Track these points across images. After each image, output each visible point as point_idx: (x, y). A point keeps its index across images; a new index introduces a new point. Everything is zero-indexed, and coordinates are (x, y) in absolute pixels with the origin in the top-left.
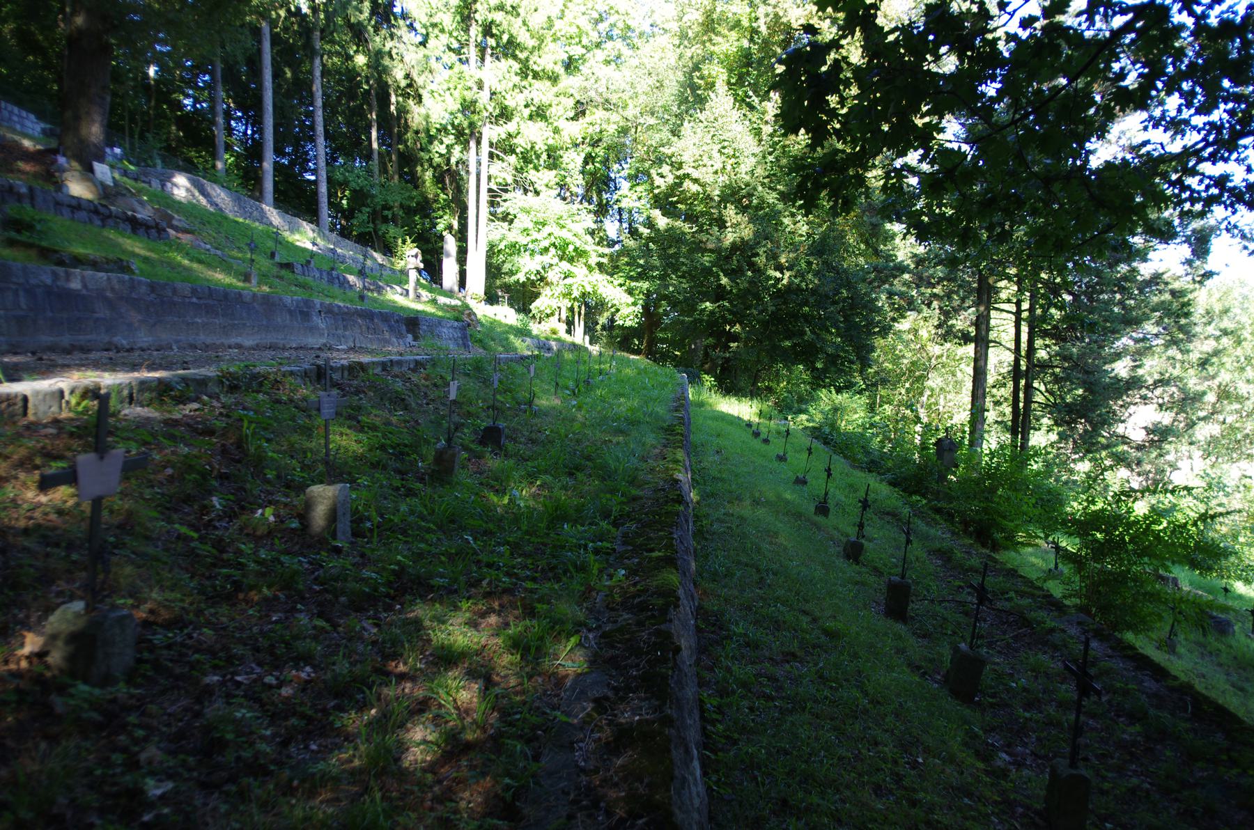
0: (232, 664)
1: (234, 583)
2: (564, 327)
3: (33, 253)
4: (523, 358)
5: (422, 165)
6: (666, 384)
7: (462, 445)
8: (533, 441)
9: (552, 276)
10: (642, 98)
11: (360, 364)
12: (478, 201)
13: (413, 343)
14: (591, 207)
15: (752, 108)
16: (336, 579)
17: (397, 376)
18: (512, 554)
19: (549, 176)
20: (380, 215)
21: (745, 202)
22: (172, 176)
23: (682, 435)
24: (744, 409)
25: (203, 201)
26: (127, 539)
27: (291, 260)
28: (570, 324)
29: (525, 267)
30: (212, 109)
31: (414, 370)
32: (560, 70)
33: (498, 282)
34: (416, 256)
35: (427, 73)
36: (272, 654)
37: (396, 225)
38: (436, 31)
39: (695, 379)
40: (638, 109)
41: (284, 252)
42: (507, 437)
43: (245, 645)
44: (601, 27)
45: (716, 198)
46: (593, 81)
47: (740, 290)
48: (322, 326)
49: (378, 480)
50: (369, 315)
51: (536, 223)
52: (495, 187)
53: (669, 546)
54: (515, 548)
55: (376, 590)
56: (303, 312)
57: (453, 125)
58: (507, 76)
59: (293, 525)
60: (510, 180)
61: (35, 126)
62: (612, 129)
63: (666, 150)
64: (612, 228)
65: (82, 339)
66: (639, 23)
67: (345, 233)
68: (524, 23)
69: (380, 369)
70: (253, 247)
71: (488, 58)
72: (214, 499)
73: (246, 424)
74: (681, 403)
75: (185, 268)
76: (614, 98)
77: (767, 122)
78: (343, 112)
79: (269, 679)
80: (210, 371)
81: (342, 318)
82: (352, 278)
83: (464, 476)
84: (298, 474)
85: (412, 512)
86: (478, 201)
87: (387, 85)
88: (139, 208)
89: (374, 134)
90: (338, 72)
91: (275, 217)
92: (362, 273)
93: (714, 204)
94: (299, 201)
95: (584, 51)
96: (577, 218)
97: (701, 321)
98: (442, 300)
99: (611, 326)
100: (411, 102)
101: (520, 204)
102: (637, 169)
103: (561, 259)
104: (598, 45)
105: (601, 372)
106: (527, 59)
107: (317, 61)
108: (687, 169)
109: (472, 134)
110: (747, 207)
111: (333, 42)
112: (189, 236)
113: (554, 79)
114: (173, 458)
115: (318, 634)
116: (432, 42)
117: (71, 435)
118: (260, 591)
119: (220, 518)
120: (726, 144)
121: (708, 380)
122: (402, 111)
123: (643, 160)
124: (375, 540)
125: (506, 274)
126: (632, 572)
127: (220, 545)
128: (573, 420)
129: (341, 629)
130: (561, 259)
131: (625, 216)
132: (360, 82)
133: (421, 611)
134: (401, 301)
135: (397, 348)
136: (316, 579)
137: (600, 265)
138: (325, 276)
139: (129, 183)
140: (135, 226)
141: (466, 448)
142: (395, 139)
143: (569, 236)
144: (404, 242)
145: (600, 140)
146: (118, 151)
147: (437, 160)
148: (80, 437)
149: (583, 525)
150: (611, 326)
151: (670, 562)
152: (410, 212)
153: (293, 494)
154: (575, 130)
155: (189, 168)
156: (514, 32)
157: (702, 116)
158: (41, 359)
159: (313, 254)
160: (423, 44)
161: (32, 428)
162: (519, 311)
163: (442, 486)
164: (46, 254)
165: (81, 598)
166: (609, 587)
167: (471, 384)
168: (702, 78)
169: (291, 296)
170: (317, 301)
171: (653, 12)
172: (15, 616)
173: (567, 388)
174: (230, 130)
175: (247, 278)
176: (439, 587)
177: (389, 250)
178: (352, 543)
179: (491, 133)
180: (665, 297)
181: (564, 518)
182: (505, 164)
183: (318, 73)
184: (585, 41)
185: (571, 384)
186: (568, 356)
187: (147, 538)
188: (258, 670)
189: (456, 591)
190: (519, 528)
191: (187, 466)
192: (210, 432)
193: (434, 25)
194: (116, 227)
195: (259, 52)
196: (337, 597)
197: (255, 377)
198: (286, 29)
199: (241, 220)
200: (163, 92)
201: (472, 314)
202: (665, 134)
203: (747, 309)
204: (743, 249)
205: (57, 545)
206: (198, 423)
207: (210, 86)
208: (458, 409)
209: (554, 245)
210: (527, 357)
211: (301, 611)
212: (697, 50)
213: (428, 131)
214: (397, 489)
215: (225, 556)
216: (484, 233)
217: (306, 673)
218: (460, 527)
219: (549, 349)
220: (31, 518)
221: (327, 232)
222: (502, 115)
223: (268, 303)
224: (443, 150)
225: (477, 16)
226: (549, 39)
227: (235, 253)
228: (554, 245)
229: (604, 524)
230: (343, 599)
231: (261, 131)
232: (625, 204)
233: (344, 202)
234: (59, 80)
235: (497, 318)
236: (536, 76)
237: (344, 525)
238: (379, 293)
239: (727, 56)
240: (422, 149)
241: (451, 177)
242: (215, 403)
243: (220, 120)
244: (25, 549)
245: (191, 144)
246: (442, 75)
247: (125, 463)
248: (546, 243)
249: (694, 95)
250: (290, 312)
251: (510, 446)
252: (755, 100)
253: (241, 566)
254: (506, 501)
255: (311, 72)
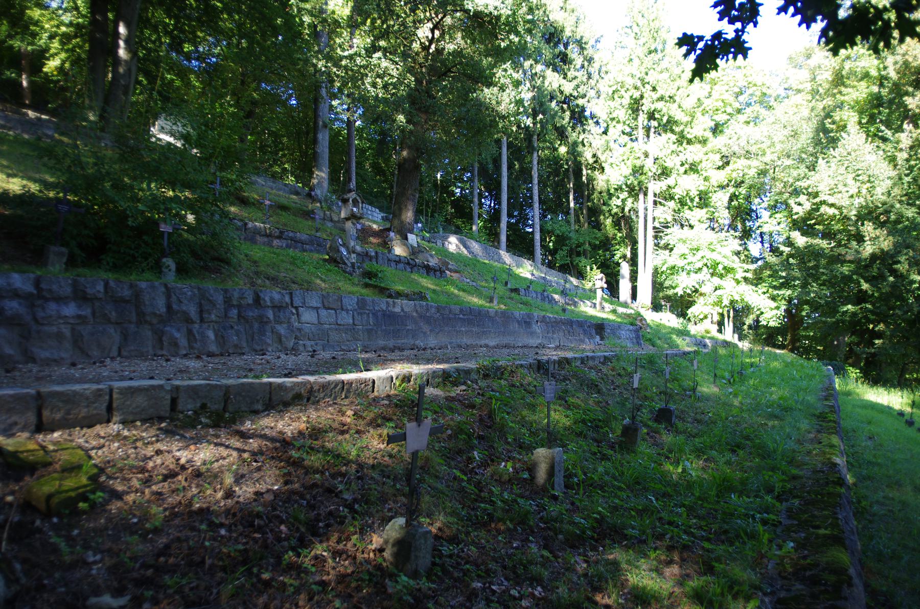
0: (489, 575)
1: (488, 515)
2: (716, 327)
3: (376, 291)
4: (685, 354)
5: (604, 215)
6: (814, 376)
7: (641, 422)
8: (699, 421)
9: (706, 289)
10: (779, 147)
11: (566, 359)
12: (645, 236)
13: (600, 342)
14: (737, 234)
15: (884, 140)
16: (555, 520)
17: (591, 368)
18: (688, 515)
19: (702, 213)
20: (576, 252)
21: (883, 218)
22: (448, 237)
23: (835, 422)
24: (895, 399)
25: (465, 252)
26: (426, 477)
27: (517, 286)
28: (721, 324)
29: (682, 284)
30: (472, 193)
31: (603, 364)
32: (709, 134)
33: (661, 295)
34: (602, 279)
35: (608, 152)
36: (515, 573)
37: (586, 258)
38: (614, 123)
39: (840, 371)
40: (776, 155)
41: (513, 281)
42: (676, 417)
43: (497, 562)
44: (741, 98)
45: (853, 218)
46: (735, 139)
47: (882, 294)
48: (539, 331)
49: (581, 446)
50: (570, 323)
51: (691, 249)
52: (658, 225)
53: (834, 525)
54: (690, 510)
55: (584, 533)
56: (526, 322)
57: (626, 184)
58: (667, 145)
59: (525, 476)
60: (670, 219)
61: (378, 215)
62: (752, 172)
63: (803, 184)
64: (755, 248)
65: (400, 342)
66: (777, 89)
67: (551, 265)
68: (680, 107)
69: (579, 362)
70: (495, 279)
71: (652, 134)
72: (475, 453)
73: (494, 402)
74: (829, 393)
75: (457, 296)
76: (753, 149)
77: (901, 150)
78: (551, 185)
79: (514, 592)
80: (472, 365)
81: (553, 325)
82: (556, 297)
83: (644, 448)
84: (527, 439)
85: (607, 473)
86: (645, 236)
87: (580, 163)
88: (431, 259)
89: (571, 197)
90: (548, 159)
91: (507, 258)
92: (563, 293)
93: (851, 223)
94: (521, 245)
95: (728, 117)
96: (725, 243)
97: (843, 322)
98: (621, 310)
99: (756, 326)
100: (596, 173)
101: (679, 237)
102: (776, 201)
103: (712, 275)
104: (739, 111)
105: (752, 365)
106: (682, 131)
107: (535, 155)
108: (822, 197)
109: (640, 189)
110: (885, 222)
111: (545, 141)
112: (457, 275)
113: (704, 142)
114: (451, 423)
115: (545, 563)
116: (611, 130)
117: (396, 405)
118: (505, 523)
119: (479, 467)
120: (860, 172)
121: (854, 373)
122: (591, 179)
123: (781, 193)
124: (581, 492)
125: (667, 288)
126: (800, 546)
127: (478, 485)
128: (732, 405)
129: (560, 560)
130: (712, 275)
131: (766, 237)
132: (562, 164)
133: (617, 554)
134: (591, 312)
135: (589, 347)
136: (541, 518)
137: (745, 279)
138: (539, 296)
139: (425, 244)
140: (428, 270)
141: (646, 425)
142: (586, 199)
143: (719, 258)
144: (591, 269)
145: (743, 182)
146: (420, 225)
147: (615, 210)
148: (401, 407)
149: (749, 497)
150: (756, 326)
151: (837, 540)
152: (595, 248)
153: (524, 453)
154: (720, 177)
155: (458, 231)
156: (672, 113)
157: (836, 153)
158: (380, 356)
159: (531, 282)
160: (605, 133)
161: (376, 400)
162: (678, 316)
163: (628, 453)
164: (383, 291)
165: (402, 515)
166: (779, 556)
167: (647, 374)
168: (834, 123)
169: (519, 311)
170: (535, 314)
171: (787, 78)
172: (367, 521)
173: (723, 378)
174: (481, 205)
175: (491, 301)
176: (631, 537)
177: (581, 275)
178: (565, 493)
179: (655, 187)
180: (807, 302)
181: (731, 489)
182: (666, 208)
183: (535, 162)
184: (729, 110)
185: (727, 375)
186: (722, 351)
187: (437, 477)
188: (506, 583)
189: (645, 542)
190: (693, 494)
191: (459, 429)
192: (473, 406)
193: (613, 119)
194: (418, 272)
195: (500, 154)
196: (556, 535)
197: (498, 368)
198: (516, 139)
199: (487, 262)
200: (444, 188)
201: (643, 320)
202: (803, 170)
203: (890, 309)
204: (884, 259)
205: (389, 477)
206: (465, 399)
207: (471, 180)
208: (638, 396)
209: (706, 265)
210: (689, 353)
211: (532, 542)
212: (829, 101)
213: (609, 190)
214: (595, 454)
215: (482, 494)
216: (650, 260)
217: (538, 591)
218: (644, 488)
219: (705, 346)
220: (375, 458)
221: (540, 266)
222: (663, 173)
223: (506, 317)
224: (619, 203)
225: (643, 108)
226: (698, 115)
227: (483, 284)
228: (706, 265)
229: (769, 498)
230: (560, 537)
231: (500, 204)
232: (765, 229)
233: (551, 244)
234: (391, 188)
235: (662, 322)
236: (689, 142)
237: (559, 479)
238: (575, 306)
239: (857, 102)
240: (604, 204)
241: (624, 221)
242: (475, 386)
243: (476, 200)
244: (372, 478)
245: (459, 216)
246: (618, 152)
247: (431, 429)
248: (700, 265)
249: (826, 137)
250: (518, 322)
251: (680, 424)
252: (888, 133)
253: (492, 503)
254: (680, 470)
255: (531, 162)
